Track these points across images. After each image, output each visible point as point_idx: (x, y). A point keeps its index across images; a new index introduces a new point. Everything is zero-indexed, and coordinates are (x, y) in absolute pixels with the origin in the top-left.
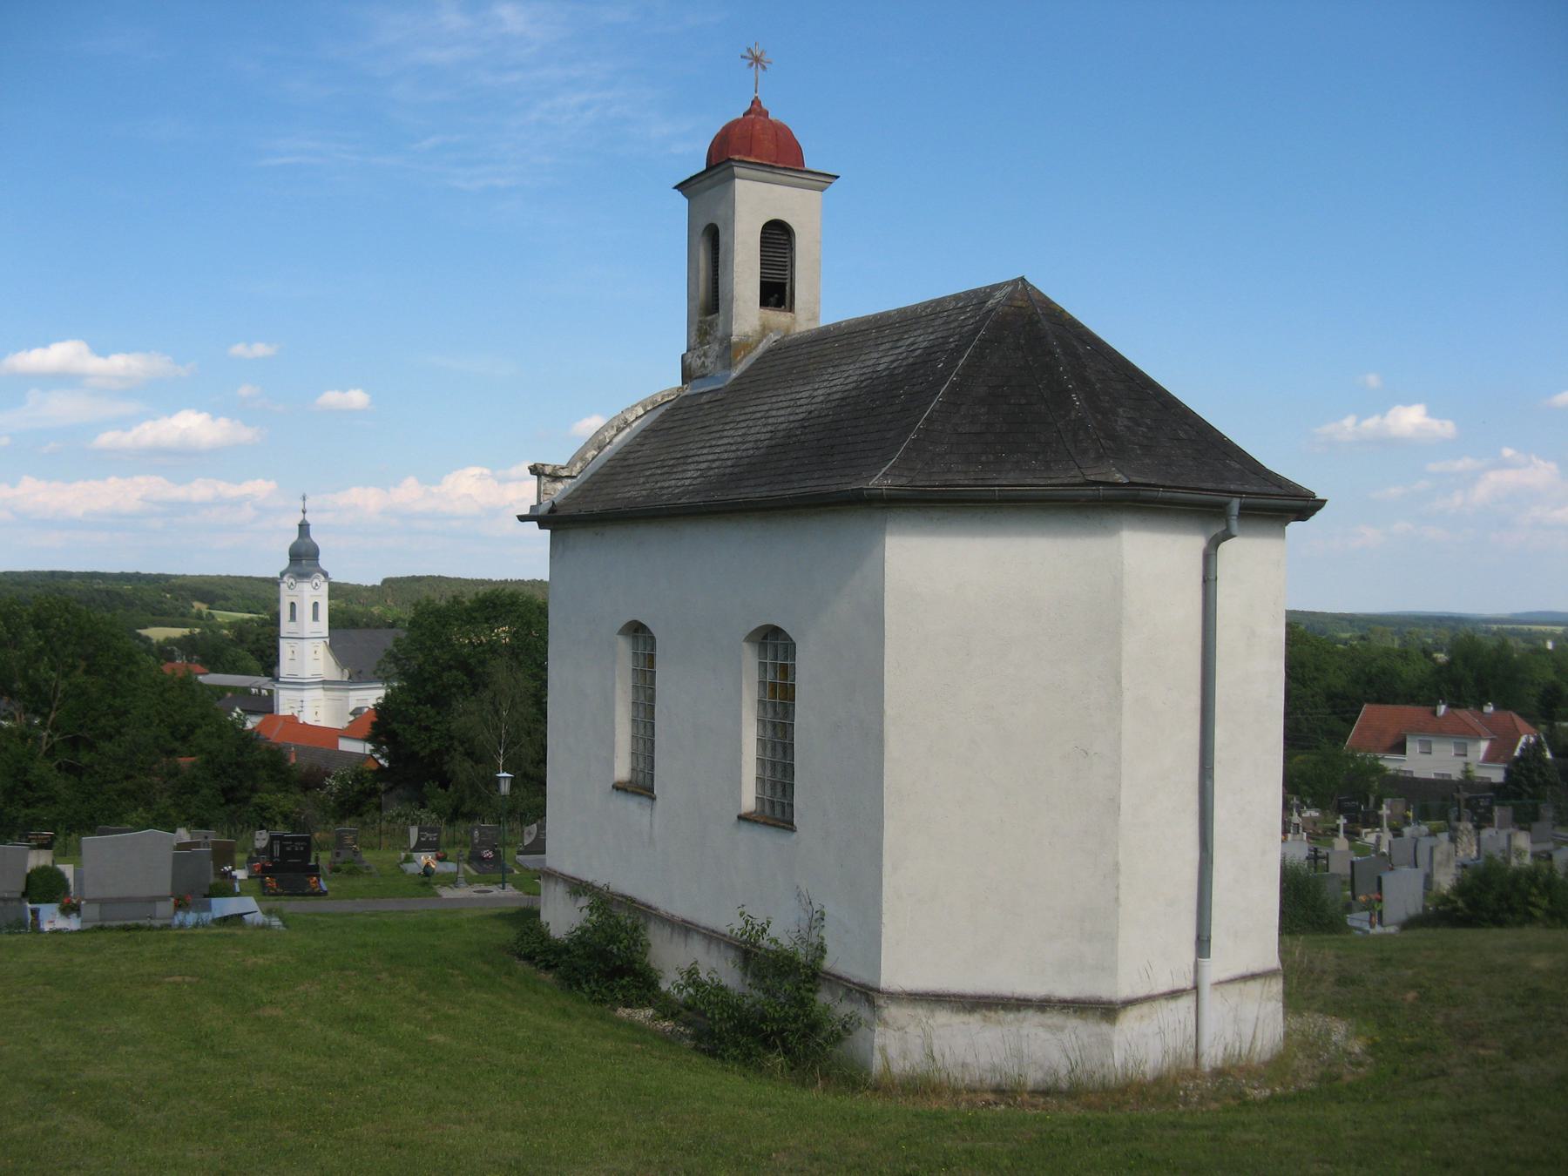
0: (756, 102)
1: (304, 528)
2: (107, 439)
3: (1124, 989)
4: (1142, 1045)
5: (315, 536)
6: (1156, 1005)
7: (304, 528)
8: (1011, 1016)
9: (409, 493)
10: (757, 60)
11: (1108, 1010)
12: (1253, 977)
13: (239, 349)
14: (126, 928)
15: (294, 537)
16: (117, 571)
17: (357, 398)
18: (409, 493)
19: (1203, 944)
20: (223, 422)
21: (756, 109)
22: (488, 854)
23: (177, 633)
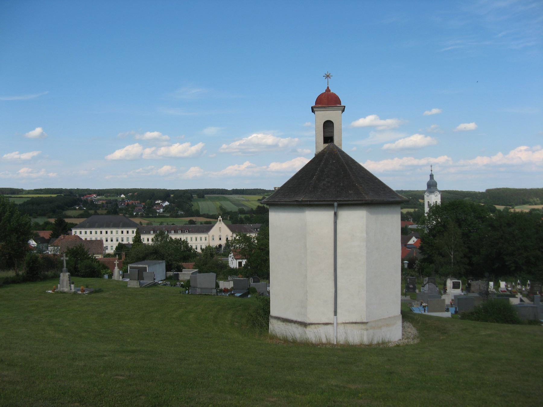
0: (328, 88)
1: (432, 176)
2: (386, 146)
3: (308, 321)
4: (312, 335)
5: (435, 178)
6: (320, 326)
7: (432, 176)
8: (290, 324)
9: (498, 158)
10: (328, 76)
11: (304, 325)
12: (356, 323)
13: (427, 113)
14: (206, 295)
15: (428, 179)
16: (400, 189)
17: (472, 126)
18: (498, 158)
19: (335, 313)
20: (429, 138)
21: (328, 90)
22: (411, 286)
23: (412, 210)
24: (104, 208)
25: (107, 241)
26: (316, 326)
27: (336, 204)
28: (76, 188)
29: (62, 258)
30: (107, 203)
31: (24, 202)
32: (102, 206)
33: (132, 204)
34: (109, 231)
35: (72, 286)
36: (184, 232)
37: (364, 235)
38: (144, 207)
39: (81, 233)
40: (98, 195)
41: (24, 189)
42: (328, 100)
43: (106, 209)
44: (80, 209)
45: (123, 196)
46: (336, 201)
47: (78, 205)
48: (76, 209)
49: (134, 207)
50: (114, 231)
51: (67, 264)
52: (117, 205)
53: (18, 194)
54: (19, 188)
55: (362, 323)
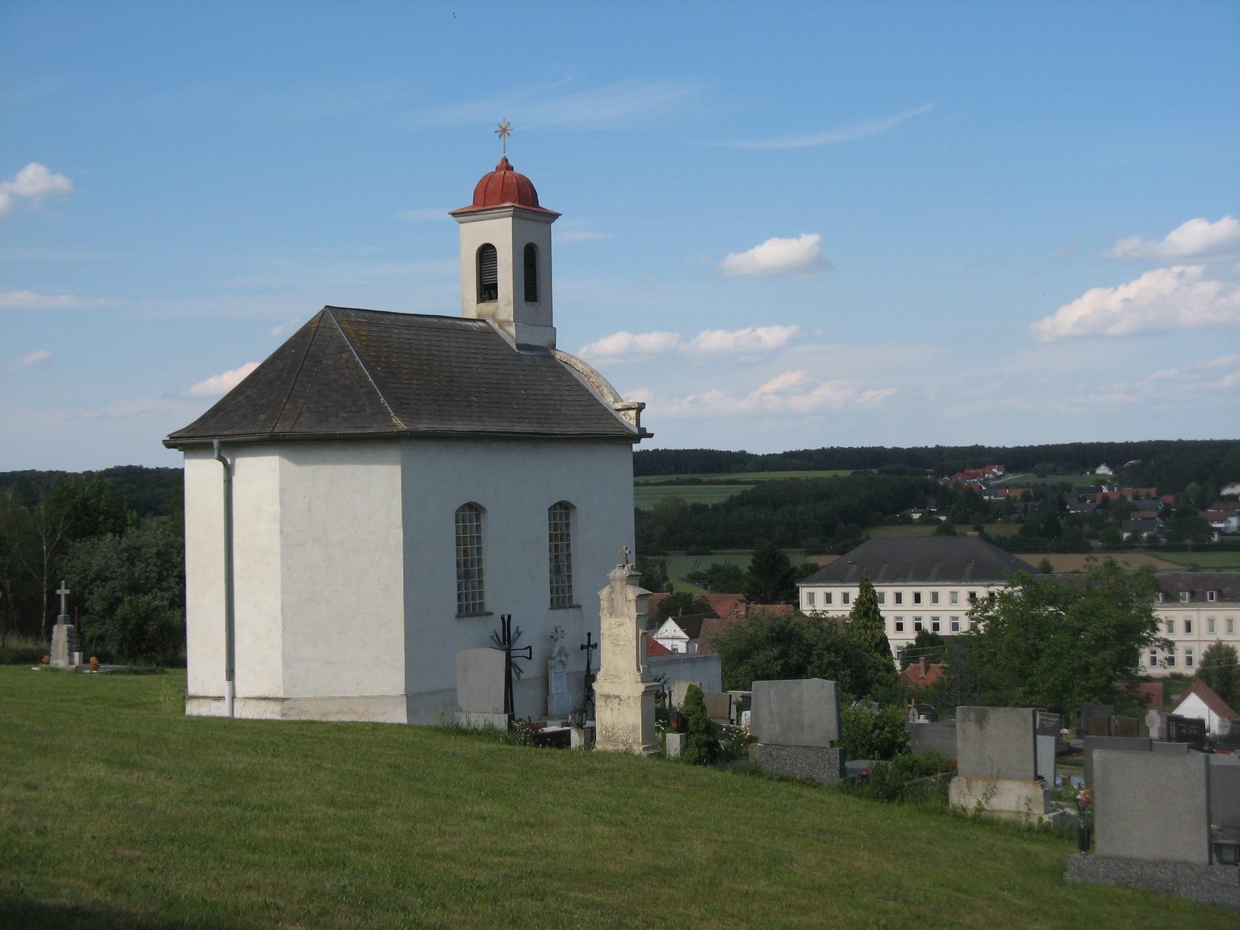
10: (504, 130)
24: (1014, 517)
25: (899, 627)
26: (202, 701)
27: (216, 442)
28: (931, 445)
29: (58, 592)
30: (1026, 497)
31: (732, 498)
32: (1008, 508)
33: (1123, 498)
34: (926, 592)
35: (76, 654)
36: (1203, 600)
37: (277, 507)
38: (1164, 514)
39: (829, 598)
40: (1009, 470)
41: (750, 451)
42: (511, 193)
43: (1018, 521)
44: (927, 520)
45: (1103, 470)
46: (214, 436)
47: (921, 506)
48: (909, 521)
49: (1124, 511)
50: (944, 591)
51: (68, 603)
52: (1062, 504)
53: (728, 471)
54: (734, 448)
55: (275, 699)
